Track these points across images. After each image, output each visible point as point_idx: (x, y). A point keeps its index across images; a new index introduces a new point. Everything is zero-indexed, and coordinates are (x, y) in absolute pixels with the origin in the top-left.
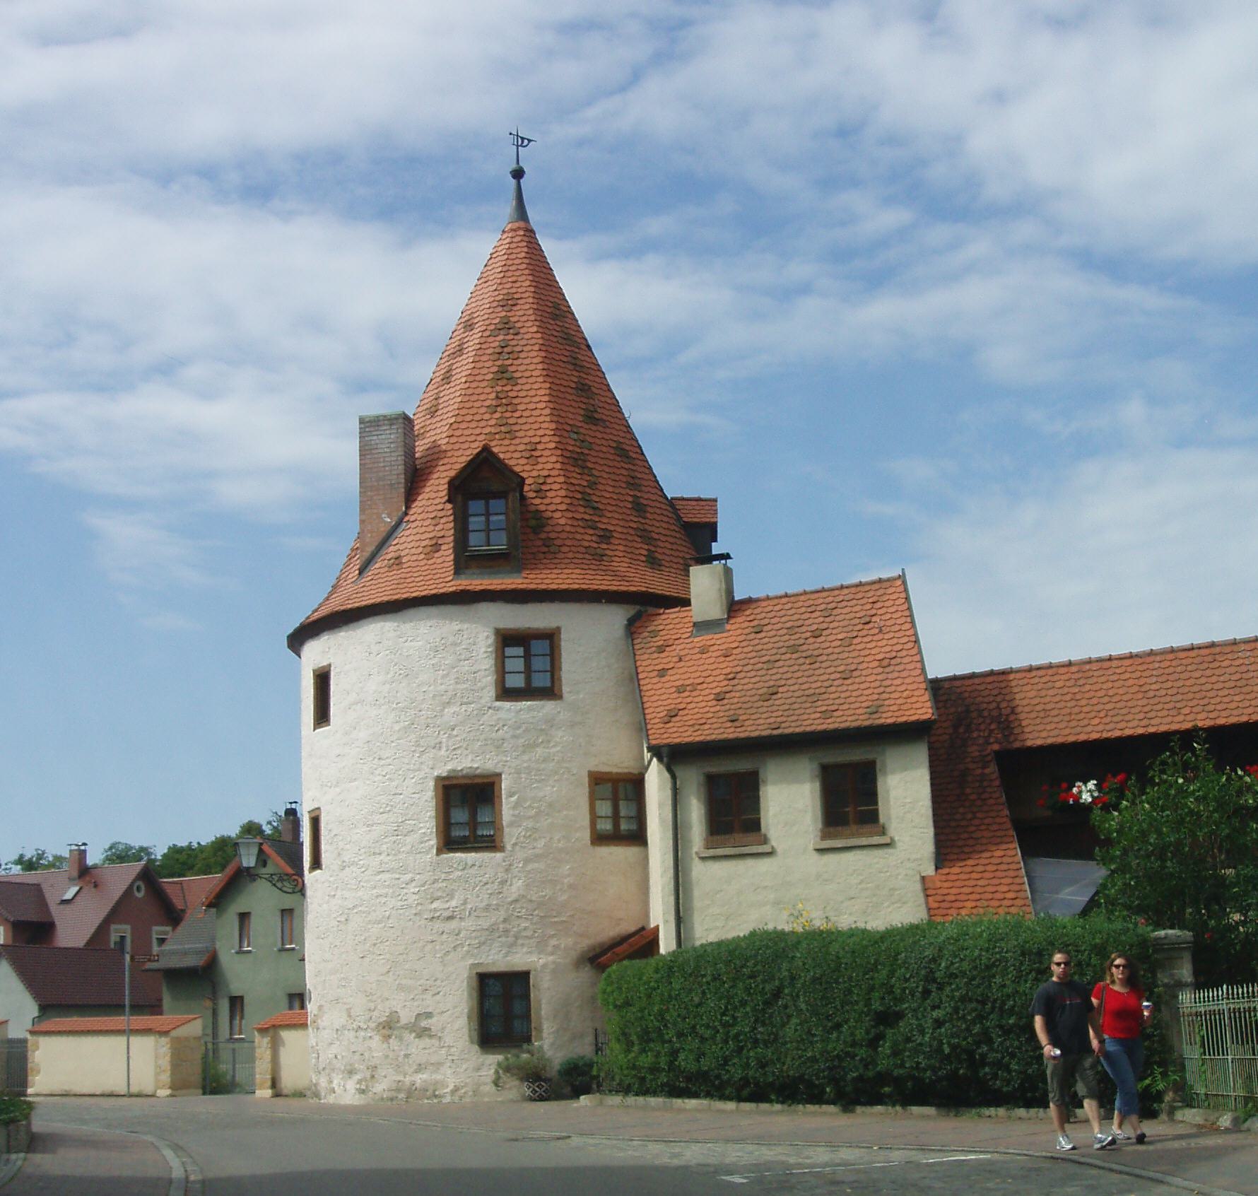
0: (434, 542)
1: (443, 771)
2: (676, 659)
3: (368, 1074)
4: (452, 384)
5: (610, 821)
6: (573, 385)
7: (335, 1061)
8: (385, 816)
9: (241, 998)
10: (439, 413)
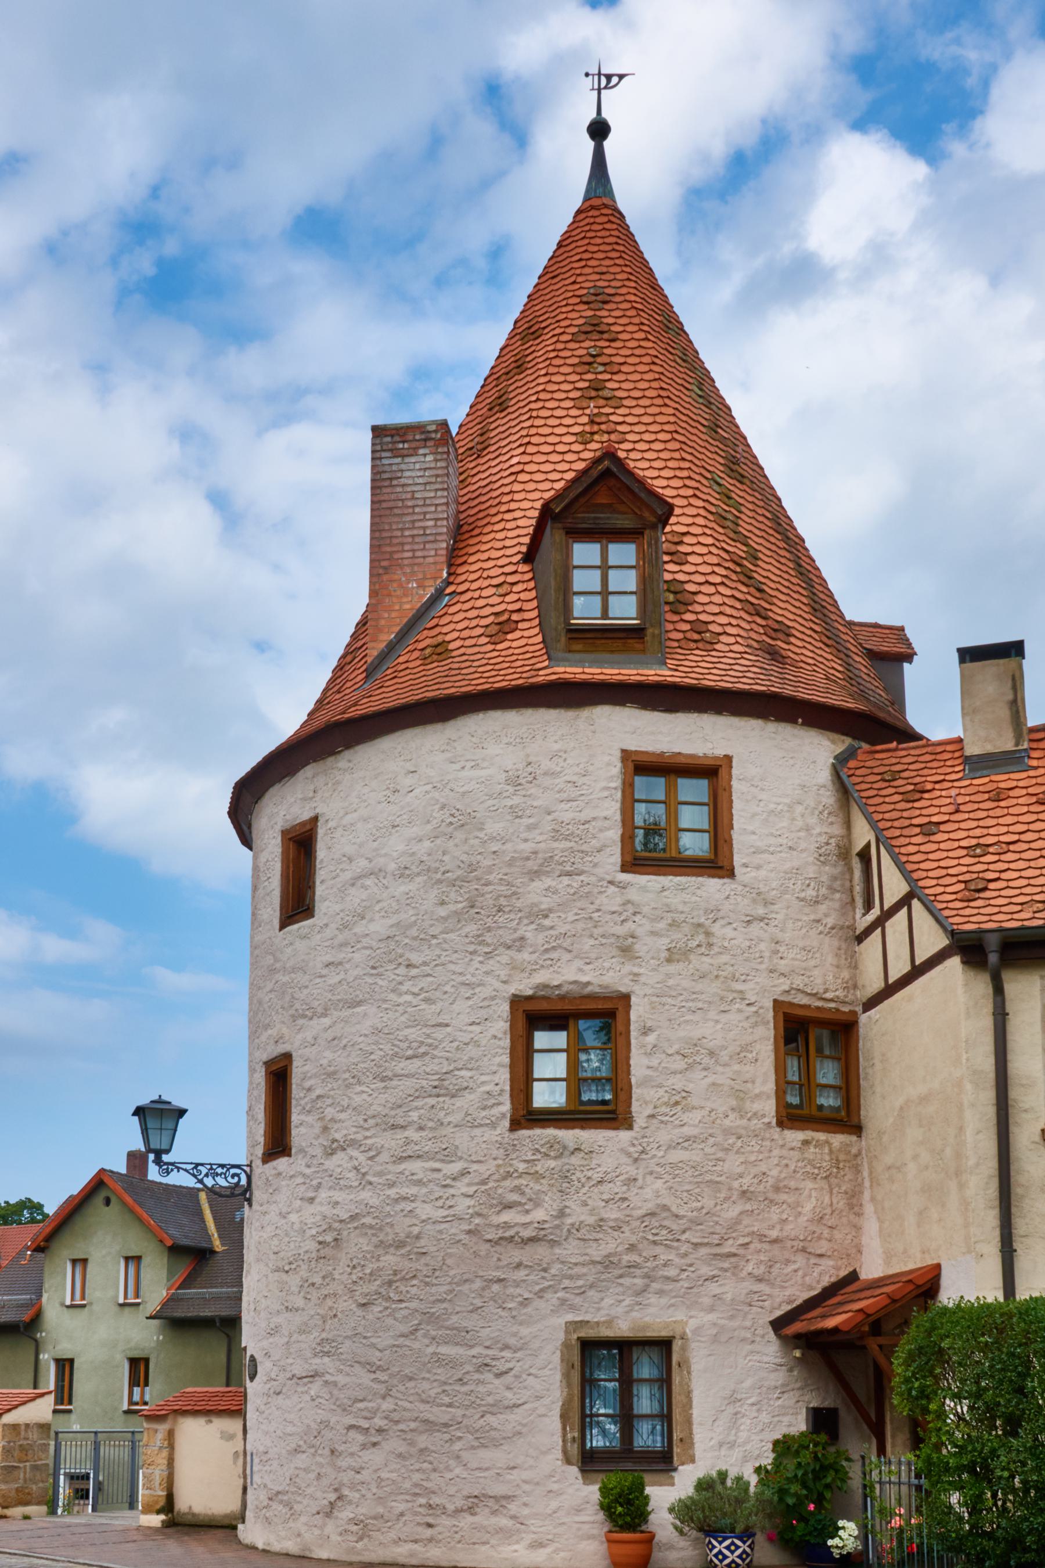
8: (417, 1062)
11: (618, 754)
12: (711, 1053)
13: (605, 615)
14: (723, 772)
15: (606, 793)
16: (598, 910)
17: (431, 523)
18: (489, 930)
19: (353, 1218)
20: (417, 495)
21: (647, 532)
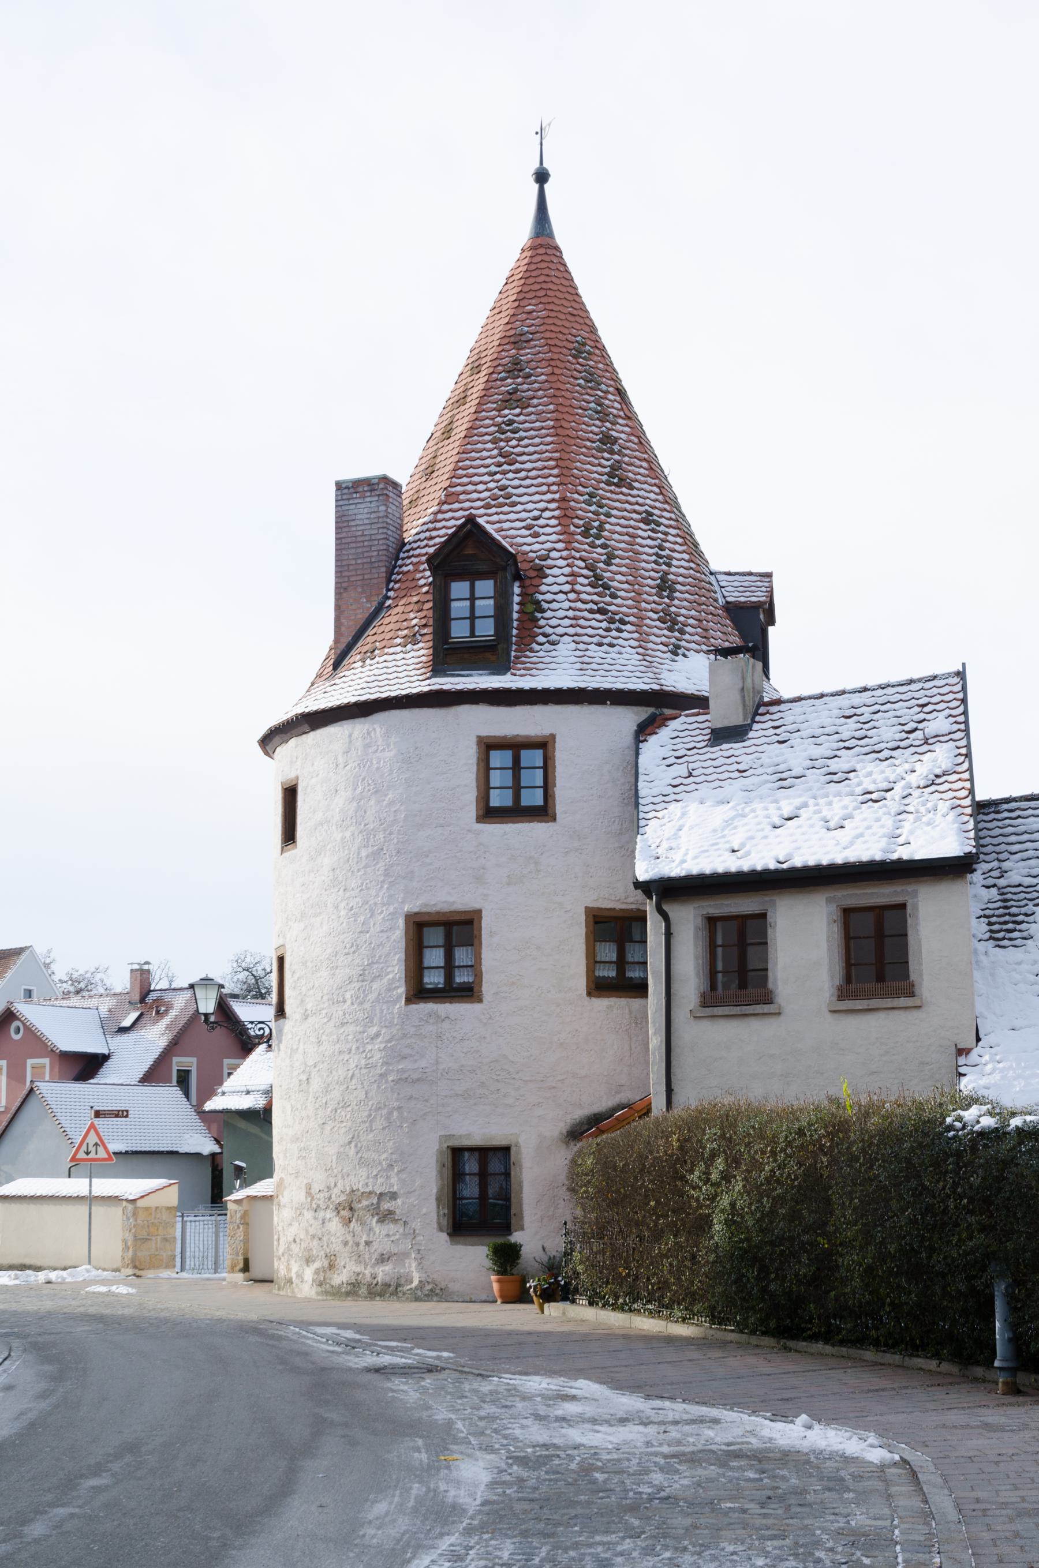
1: (414, 906)
3: (326, 1264)
5: (614, 966)
10: (434, 475)
11: (474, 740)
13: (472, 634)
14: (549, 747)
16: (461, 851)
17: (375, 553)
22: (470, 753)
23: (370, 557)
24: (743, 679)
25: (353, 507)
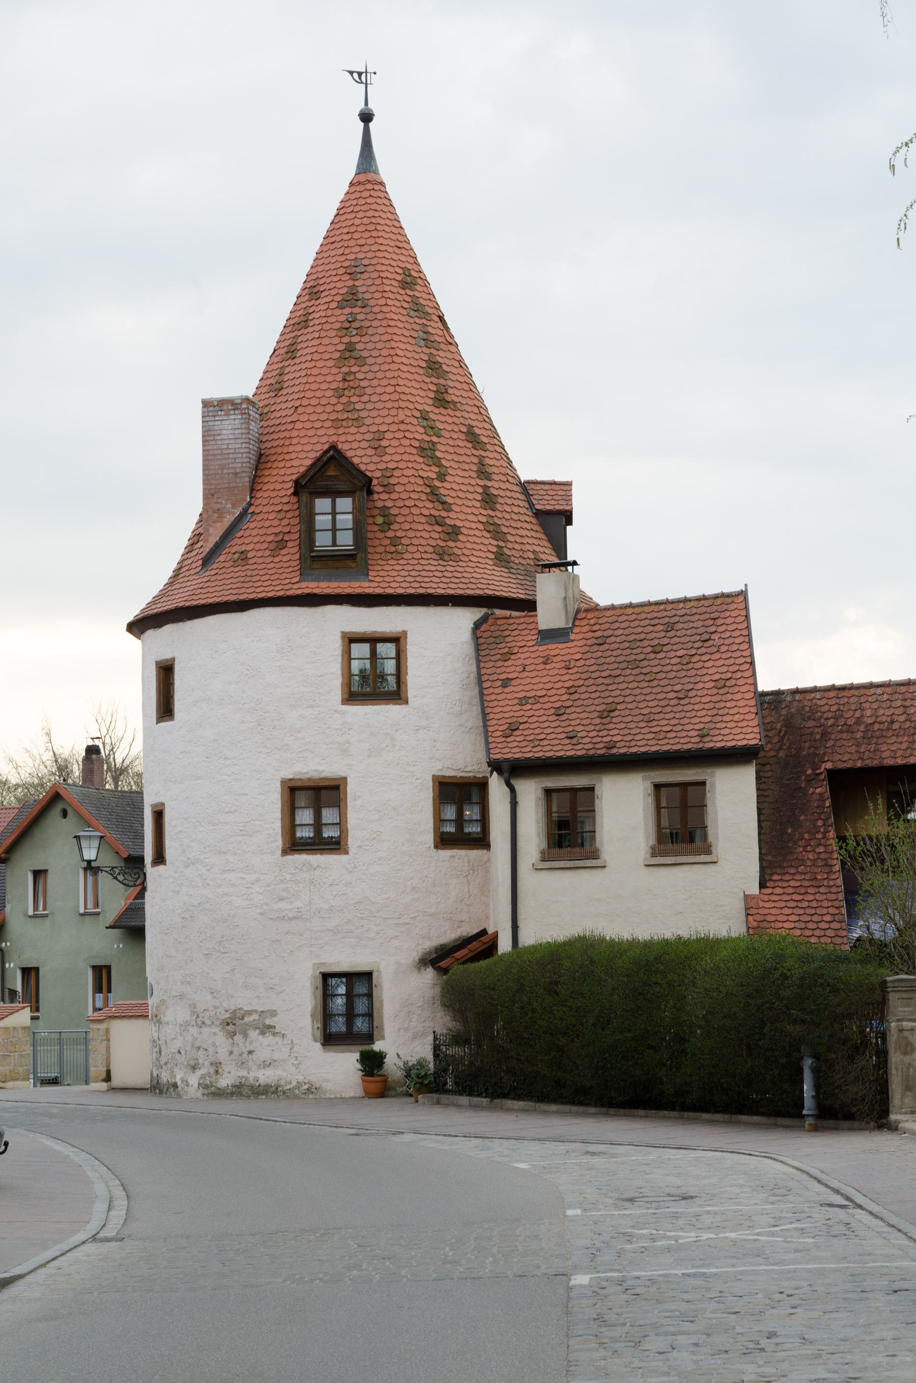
0: (280, 537)
2: (519, 669)
3: (212, 1070)
4: (297, 361)
5: (453, 824)
6: (424, 365)
7: (178, 1056)
9: (37, 969)
10: (284, 392)
11: (339, 635)
12: (394, 809)
13: (334, 543)
14: (402, 640)
15: (332, 659)
17: (240, 465)
18: (268, 739)
19: (200, 904)
20: (230, 446)
21: (358, 493)
22: (336, 646)
23: (235, 468)
24: (566, 590)
25: (219, 423)
